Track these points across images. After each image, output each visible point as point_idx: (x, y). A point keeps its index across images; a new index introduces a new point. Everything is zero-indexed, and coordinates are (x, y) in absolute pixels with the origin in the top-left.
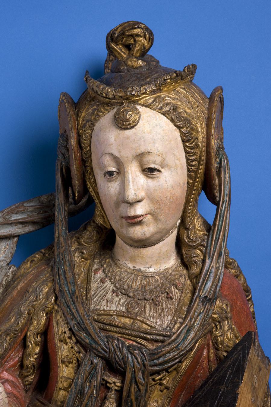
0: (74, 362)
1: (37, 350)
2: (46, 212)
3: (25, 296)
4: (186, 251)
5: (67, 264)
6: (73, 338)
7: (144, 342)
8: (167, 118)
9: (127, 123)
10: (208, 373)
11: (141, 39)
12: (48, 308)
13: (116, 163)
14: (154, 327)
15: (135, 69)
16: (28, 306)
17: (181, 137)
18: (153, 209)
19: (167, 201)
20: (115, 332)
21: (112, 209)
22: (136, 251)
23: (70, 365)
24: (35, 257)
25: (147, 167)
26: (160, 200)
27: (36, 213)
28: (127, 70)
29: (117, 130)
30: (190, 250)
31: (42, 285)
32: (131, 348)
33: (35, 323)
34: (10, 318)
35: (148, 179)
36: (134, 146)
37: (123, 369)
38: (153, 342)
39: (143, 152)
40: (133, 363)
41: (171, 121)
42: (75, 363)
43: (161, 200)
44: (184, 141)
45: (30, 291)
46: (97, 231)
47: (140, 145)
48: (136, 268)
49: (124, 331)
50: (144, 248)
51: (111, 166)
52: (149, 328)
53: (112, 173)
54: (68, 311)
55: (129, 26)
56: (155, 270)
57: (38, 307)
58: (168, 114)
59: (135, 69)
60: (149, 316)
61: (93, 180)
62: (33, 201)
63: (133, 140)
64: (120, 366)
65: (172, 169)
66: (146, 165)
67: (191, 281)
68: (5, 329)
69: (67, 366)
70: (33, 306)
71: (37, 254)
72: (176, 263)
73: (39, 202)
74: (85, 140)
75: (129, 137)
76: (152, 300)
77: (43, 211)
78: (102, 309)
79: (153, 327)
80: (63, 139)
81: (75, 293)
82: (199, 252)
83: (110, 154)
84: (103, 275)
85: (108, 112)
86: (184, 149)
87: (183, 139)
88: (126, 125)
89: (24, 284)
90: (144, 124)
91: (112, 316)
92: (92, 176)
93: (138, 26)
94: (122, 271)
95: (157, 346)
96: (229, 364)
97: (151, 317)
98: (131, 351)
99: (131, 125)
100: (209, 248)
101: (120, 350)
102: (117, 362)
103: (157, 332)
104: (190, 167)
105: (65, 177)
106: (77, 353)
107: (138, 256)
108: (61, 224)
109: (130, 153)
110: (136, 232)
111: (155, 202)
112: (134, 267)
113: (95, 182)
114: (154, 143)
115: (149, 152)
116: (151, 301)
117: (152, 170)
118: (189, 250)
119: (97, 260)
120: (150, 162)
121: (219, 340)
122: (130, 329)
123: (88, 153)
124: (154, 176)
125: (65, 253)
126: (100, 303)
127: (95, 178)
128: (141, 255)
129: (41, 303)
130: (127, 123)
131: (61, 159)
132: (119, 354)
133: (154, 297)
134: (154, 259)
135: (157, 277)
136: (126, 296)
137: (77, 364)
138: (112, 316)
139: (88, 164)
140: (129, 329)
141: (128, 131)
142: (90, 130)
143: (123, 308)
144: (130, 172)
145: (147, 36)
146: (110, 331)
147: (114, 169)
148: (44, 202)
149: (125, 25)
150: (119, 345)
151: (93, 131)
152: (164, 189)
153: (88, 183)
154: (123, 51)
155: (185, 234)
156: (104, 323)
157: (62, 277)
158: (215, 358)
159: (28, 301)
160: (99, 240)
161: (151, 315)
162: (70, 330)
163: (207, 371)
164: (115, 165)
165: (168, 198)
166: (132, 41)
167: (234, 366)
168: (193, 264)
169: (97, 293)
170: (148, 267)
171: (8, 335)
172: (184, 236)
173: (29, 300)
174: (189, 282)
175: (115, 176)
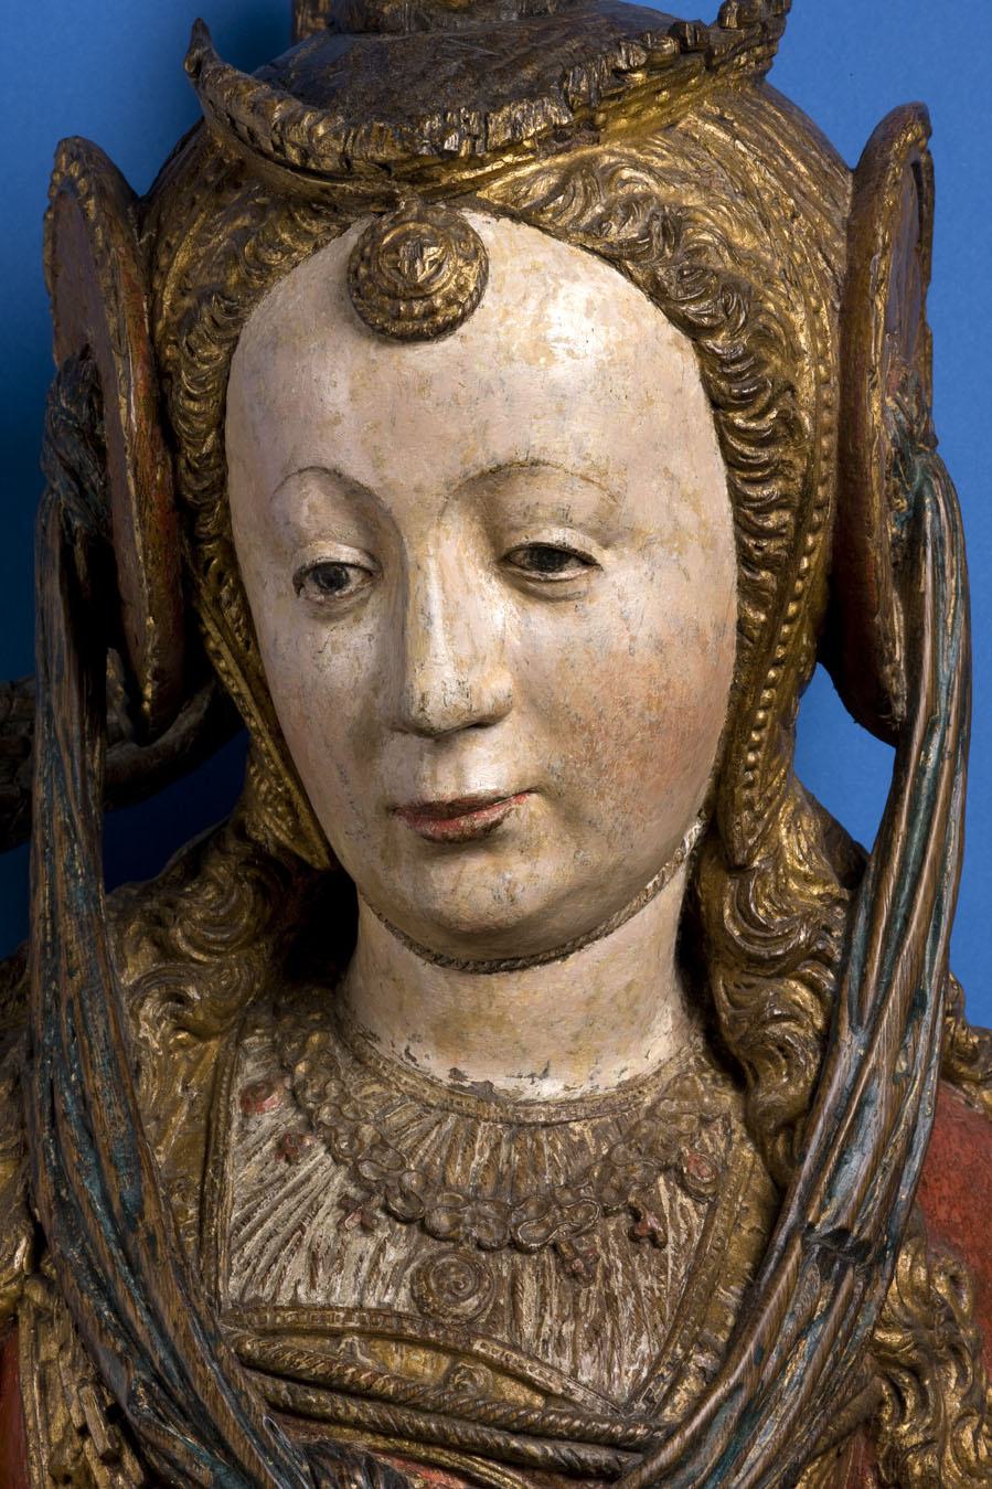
4: (732, 988)
5: (98, 1060)
6: (129, 1461)
9: (418, 308)
14: (562, 1397)
17: (705, 381)
18: (557, 764)
20: (357, 1425)
28: (418, 18)
29: (365, 344)
30: (754, 980)
35: (529, 606)
36: (453, 430)
39: (501, 460)
41: (652, 296)
43: (601, 715)
44: (717, 404)
46: (257, 882)
47: (486, 426)
48: (464, 1078)
52: (538, 1401)
53: (337, 573)
54: (99, 1314)
58: (633, 257)
60: (538, 1336)
61: (234, 609)
66: (517, 529)
67: (760, 1148)
74: (191, 397)
75: (424, 384)
76: (555, 1248)
78: (284, 1299)
81: (142, 1216)
82: (802, 994)
83: (325, 470)
85: (317, 248)
86: (723, 442)
87: (715, 392)
90: (507, 313)
91: (337, 1335)
92: (233, 592)
104: (751, 542)
109: (433, 464)
110: (466, 888)
111: (565, 727)
112: (455, 1073)
113: (250, 625)
114: (560, 411)
115: (535, 463)
116: (548, 1258)
117: (551, 557)
120: (540, 512)
121: (917, 1470)
122: (437, 1410)
124: (546, 589)
126: (275, 1269)
127: (245, 599)
128: (494, 1012)
130: (418, 308)
134: (565, 1031)
136: (415, 1227)
138: (337, 1335)
141: (424, 348)
142: (221, 343)
146: (325, 1419)
147: (347, 554)
152: (612, 655)
155: (728, 900)
156: (293, 1378)
157: (71, 1130)
161: (545, 1329)
162: (114, 1415)
164: (354, 532)
165: (637, 706)
168: (773, 1059)
169: (257, 1216)
170: (532, 1076)
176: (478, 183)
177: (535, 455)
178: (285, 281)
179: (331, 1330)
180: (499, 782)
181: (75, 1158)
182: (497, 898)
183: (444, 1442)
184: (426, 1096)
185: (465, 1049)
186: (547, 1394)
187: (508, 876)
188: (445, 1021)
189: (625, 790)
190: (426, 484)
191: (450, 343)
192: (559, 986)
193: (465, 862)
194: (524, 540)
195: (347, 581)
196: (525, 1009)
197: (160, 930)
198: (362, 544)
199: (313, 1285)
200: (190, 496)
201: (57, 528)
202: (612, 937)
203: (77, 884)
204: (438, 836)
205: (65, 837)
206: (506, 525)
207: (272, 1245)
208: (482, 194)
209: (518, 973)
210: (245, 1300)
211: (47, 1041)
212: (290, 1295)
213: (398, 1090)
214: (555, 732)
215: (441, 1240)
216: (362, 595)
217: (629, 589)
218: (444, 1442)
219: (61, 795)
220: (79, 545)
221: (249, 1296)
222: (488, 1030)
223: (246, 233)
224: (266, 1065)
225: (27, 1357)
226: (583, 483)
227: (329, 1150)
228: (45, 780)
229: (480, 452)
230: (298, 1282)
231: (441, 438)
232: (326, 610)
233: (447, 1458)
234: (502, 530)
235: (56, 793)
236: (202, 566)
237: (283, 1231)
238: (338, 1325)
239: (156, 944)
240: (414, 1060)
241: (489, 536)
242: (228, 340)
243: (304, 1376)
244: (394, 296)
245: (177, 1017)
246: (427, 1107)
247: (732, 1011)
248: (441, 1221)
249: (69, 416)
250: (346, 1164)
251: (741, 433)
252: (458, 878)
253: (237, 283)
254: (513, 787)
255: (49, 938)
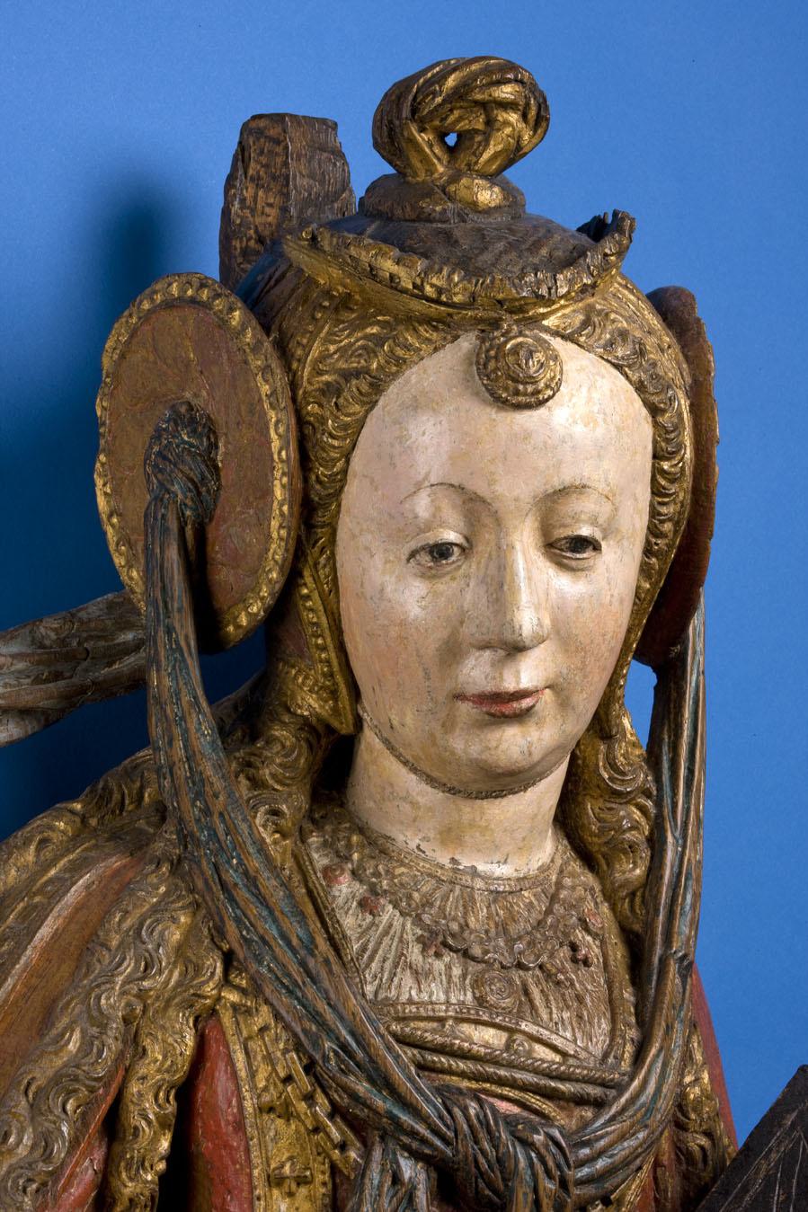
0: (320, 1178)
1: (165, 1144)
2: (57, 676)
3: (99, 961)
4: (597, 810)
5: (251, 851)
6: (320, 1098)
7: (547, 1107)
8: (627, 377)
9: (530, 389)
10: (653, 1204)
11: (513, 117)
12: (205, 997)
13: (465, 517)
14: (574, 1056)
15: (480, 212)
16: (123, 993)
17: (655, 442)
18: (565, 671)
19: (603, 648)
20: (463, 1075)
21: (425, 669)
22: (468, 809)
23: (303, 1191)
24: (52, 828)
25: (568, 532)
26: (588, 641)
27: (29, 677)
28: (459, 215)
29: (488, 409)
30: (614, 806)
31: (158, 921)
32: (520, 1127)
33: (155, 1052)
34: (62, 1035)
35: (561, 574)
36: (541, 465)
37: (498, 1196)
38: (572, 1105)
39: (567, 484)
40: (534, 1176)
41: (637, 389)
42: (324, 1184)
43: (592, 642)
45: (114, 943)
46: (308, 741)
47: (560, 462)
48: (459, 864)
49: (491, 1070)
50: (496, 797)
51: (450, 528)
52: (558, 1058)
53: (448, 549)
54: (295, 1007)
55: (487, 71)
56: (516, 870)
57: (158, 998)
58: (629, 366)
59: (480, 212)
60: (551, 1020)
61: (327, 570)
62: (16, 637)
63: (541, 445)
64: (490, 1185)
65: (625, 543)
66: (564, 526)
67: (613, 908)
68: (50, 1073)
69: (291, 1194)
70: (142, 995)
71: (58, 819)
72: (557, 849)
73: (33, 642)
74: (333, 437)
75: (527, 436)
76: (541, 967)
77: (50, 673)
78: (404, 998)
79: (570, 1056)
80: (194, 431)
81: (316, 947)
82: (637, 815)
83: (452, 486)
84: (361, 890)
85: (436, 350)
86: (653, 479)
87: (658, 449)
88: (525, 394)
89: (61, 920)
90: (572, 395)
92: (328, 559)
93: (516, 76)
94: (415, 876)
95: (582, 1117)
96: (768, 1171)
97: (556, 1024)
98: (521, 1135)
99: (541, 397)
100: (667, 801)
101: (489, 1132)
102: (482, 1174)
103: (585, 1072)
104: (654, 540)
105: (193, 558)
106: (335, 1147)
107: (472, 825)
108: (194, 715)
109: (527, 485)
110: (504, 746)
111: (573, 648)
112: (453, 861)
113: (335, 580)
114: (599, 456)
116: (538, 972)
117: (580, 544)
118: (609, 805)
119: (315, 839)
120: (583, 517)
121: (692, 1096)
123: (334, 481)
124: (573, 563)
125: (232, 815)
126: (396, 980)
127: (334, 564)
128: (483, 823)
129: (167, 982)
130: (530, 389)
131: (180, 496)
132: (486, 1146)
133: (544, 958)
134: (519, 835)
135: (526, 894)
136: (460, 954)
137: (330, 1186)
138: (442, 1020)
139: (321, 517)
140: (505, 1062)
141: (527, 414)
142: (363, 404)
143: (465, 995)
144: (518, 546)
145: (533, 113)
146: (443, 1071)
147: (451, 536)
148: (47, 642)
149: (474, 67)
150: (486, 1115)
151: (372, 409)
152: (602, 605)
153: (308, 579)
154: (436, 151)
155: (601, 757)
157: (243, 894)
158: (673, 1157)
159: (121, 978)
160: (308, 773)
161: (554, 1016)
162: (309, 1068)
163: (652, 1197)
164: (462, 524)
165: (608, 637)
166: (479, 124)
167: (788, 1175)
168: (625, 853)
169: (370, 946)
170: (499, 862)
171: (70, 1093)
172: (597, 760)
173: (121, 974)
174: (605, 908)
175: (453, 558)
176: (545, 316)
177: (584, 482)
178: (415, 369)
179: (439, 1017)
180: (531, 680)
181: (255, 911)
182: (522, 752)
183: (513, 1084)
184: (438, 874)
185: (461, 845)
186: (564, 1054)
187: (529, 739)
188: (450, 829)
189: (592, 688)
190: (522, 496)
191: (542, 411)
192: (521, 807)
193: (504, 731)
194: (570, 533)
195: (451, 555)
196: (501, 821)
197: (252, 771)
198: (465, 532)
199: (420, 991)
200: (316, 499)
201: (175, 516)
202: (549, 778)
203: (205, 740)
204: (498, 714)
205: (192, 711)
206: (558, 524)
207: (388, 965)
208: (545, 323)
209: (499, 799)
210: (379, 999)
211: (203, 838)
212: (407, 996)
213: (419, 871)
214: (567, 651)
215: (479, 962)
216: (459, 563)
217: (611, 566)
218: (513, 1084)
219: (185, 684)
220: (190, 527)
221: (381, 996)
222: (478, 834)
223: (379, 341)
224: (327, 855)
225: (233, 1035)
226: (606, 500)
227: (394, 907)
228: (169, 674)
229: (556, 479)
230: (411, 988)
231: (534, 469)
232: (433, 572)
233: (512, 1094)
234: (554, 527)
235: (181, 683)
236: (312, 542)
237: (391, 956)
238: (442, 1014)
239: (248, 778)
240: (424, 852)
241: (542, 530)
242: (368, 403)
243: (428, 1045)
244: (516, 380)
245: (276, 825)
246: (440, 881)
247: (599, 824)
248: (477, 951)
249: (191, 445)
250: (411, 916)
251: (663, 472)
252: (500, 739)
253: (377, 368)
254: (541, 684)
255: (188, 774)
